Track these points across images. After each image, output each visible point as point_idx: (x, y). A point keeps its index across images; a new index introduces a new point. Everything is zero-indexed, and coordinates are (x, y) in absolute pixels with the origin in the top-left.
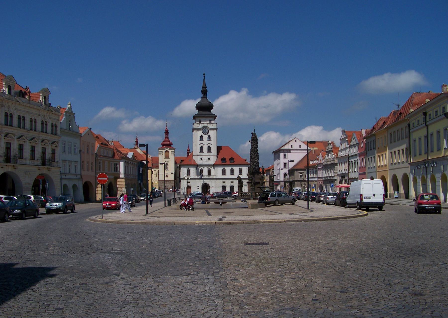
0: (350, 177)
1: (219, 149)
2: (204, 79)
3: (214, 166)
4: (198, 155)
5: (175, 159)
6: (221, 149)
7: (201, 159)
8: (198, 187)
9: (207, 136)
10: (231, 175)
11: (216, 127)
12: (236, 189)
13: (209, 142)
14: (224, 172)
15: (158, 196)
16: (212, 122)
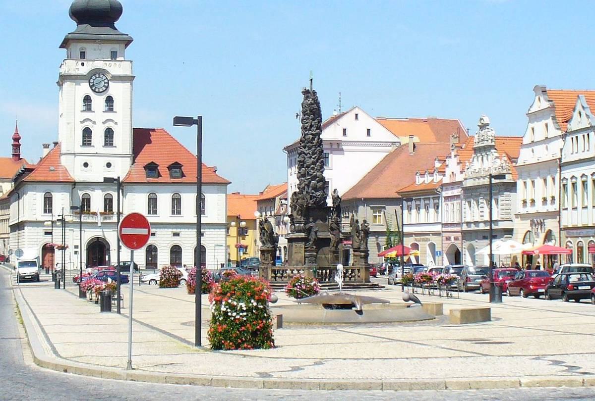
0: (564, 224)
10: (173, 213)
11: (129, 73)
12: (188, 258)
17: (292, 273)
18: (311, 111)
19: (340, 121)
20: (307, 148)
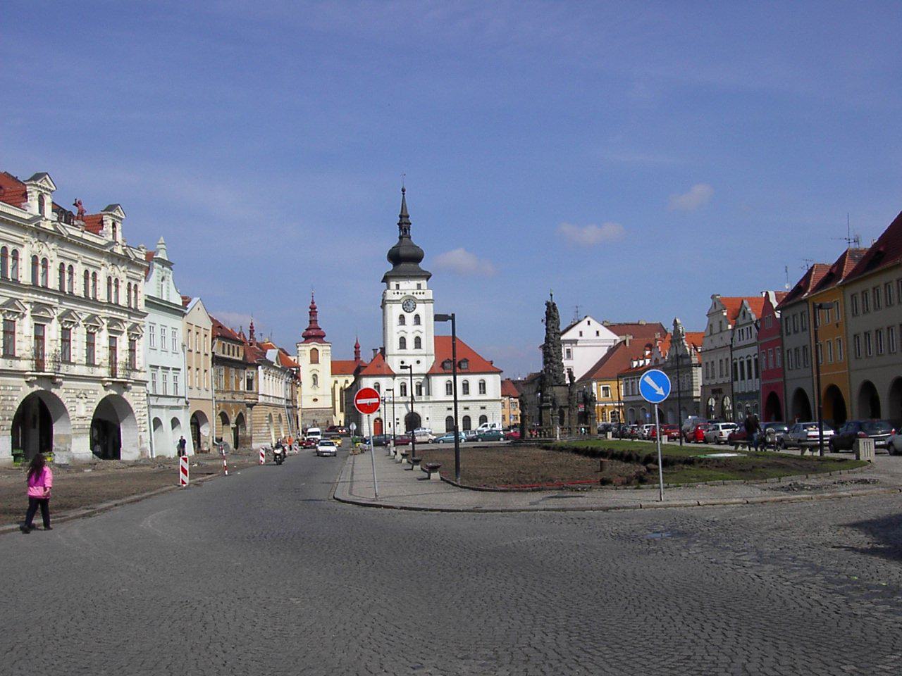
4: (394, 355)
9: (413, 314)
10: (480, 393)
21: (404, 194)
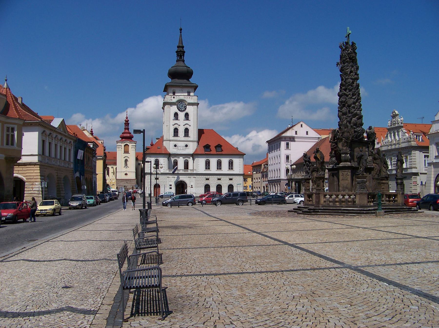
1: (201, 132)
2: (181, 36)
3: (194, 156)
4: (170, 141)
5: (136, 153)
6: (204, 133)
7: (175, 146)
8: (171, 185)
13: (187, 122)
14: (208, 165)
15: (111, 199)
16: (192, 94)
17: (343, 197)
18: (350, 59)
19: (294, 128)
20: (348, 91)
21: (181, 32)
